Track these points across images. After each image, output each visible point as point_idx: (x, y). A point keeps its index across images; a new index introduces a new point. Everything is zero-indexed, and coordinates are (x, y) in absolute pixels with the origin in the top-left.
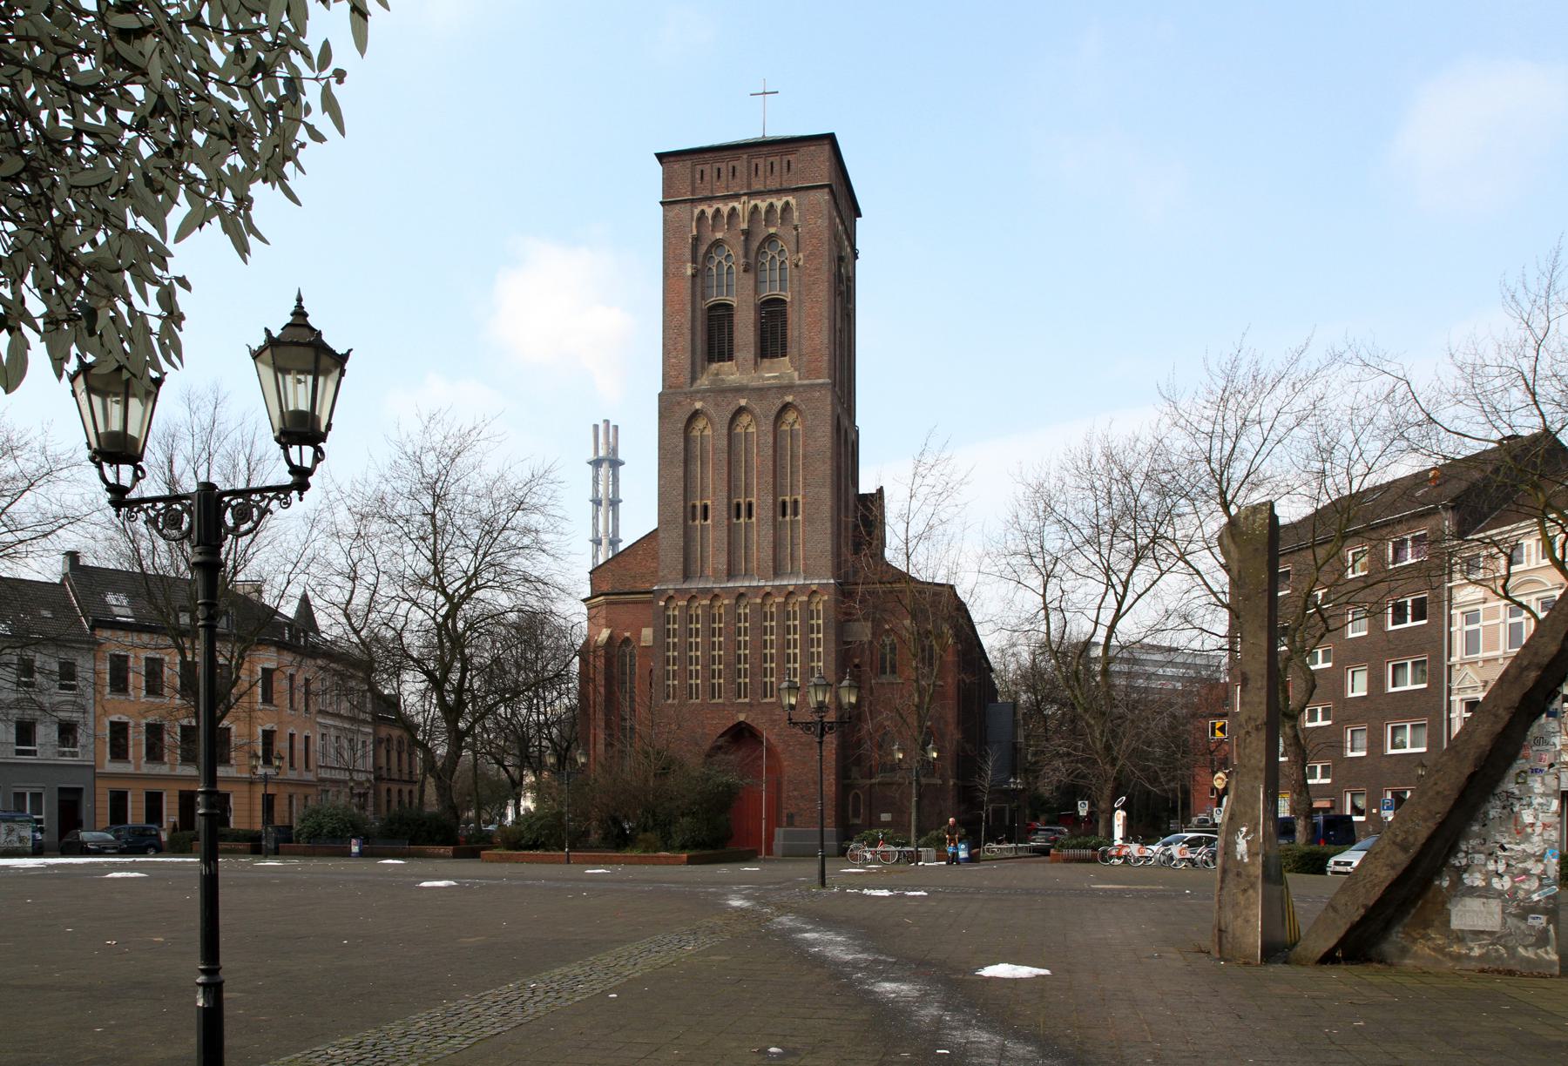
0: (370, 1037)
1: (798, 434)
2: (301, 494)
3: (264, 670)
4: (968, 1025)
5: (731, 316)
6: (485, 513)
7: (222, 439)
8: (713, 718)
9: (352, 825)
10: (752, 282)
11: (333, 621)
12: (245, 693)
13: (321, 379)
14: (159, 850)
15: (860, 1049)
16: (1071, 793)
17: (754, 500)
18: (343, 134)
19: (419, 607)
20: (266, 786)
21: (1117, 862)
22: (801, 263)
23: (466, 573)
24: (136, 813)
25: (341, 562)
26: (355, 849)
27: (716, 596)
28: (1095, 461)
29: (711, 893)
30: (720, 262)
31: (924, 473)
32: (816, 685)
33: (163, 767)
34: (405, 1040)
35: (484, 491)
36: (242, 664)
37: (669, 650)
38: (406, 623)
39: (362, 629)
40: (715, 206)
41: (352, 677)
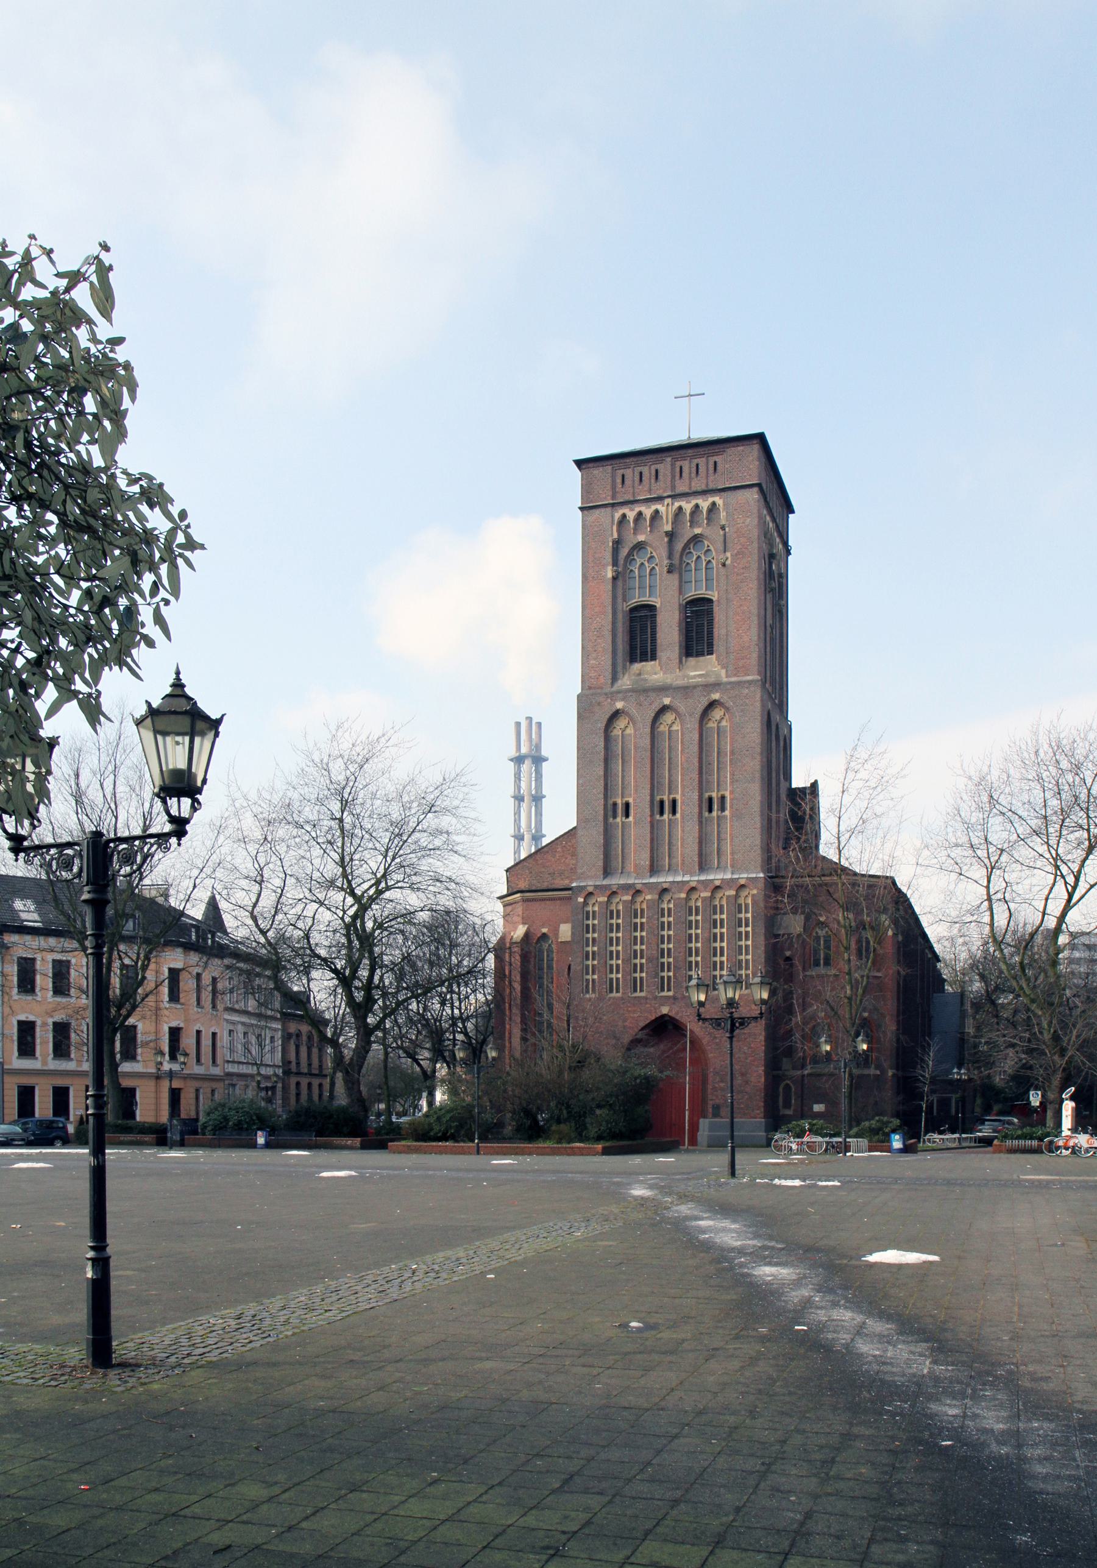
0: (251, 1308)
1: (725, 732)
2: (179, 840)
3: (170, 969)
4: (835, 1304)
5: (655, 616)
6: (395, 816)
7: (128, 751)
8: (634, 1012)
9: (259, 1118)
10: (677, 583)
11: (240, 923)
12: (151, 992)
13: (197, 740)
14: (66, 1141)
15: (720, 1325)
16: (1023, 1081)
17: (678, 797)
18: (170, 640)
19: (327, 908)
20: (171, 1081)
21: (1065, 1152)
22: (728, 562)
23: (375, 874)
24: (43, 1107)
25: (248, 867)
26: (261, 1140)
27: (638, 892)
28: (1041, 753)
29: (614, 1183)
30: (642, 564)
31: (856, 768)
32: (725, 982)
33: (70, 1063)
34: (284, 1312)
35: (395, 794)
36: (148, 965)
37: (588, 945)
38: (313, 924)
39: (268, 930)
40: (637, 510)
41: (258, 975)
